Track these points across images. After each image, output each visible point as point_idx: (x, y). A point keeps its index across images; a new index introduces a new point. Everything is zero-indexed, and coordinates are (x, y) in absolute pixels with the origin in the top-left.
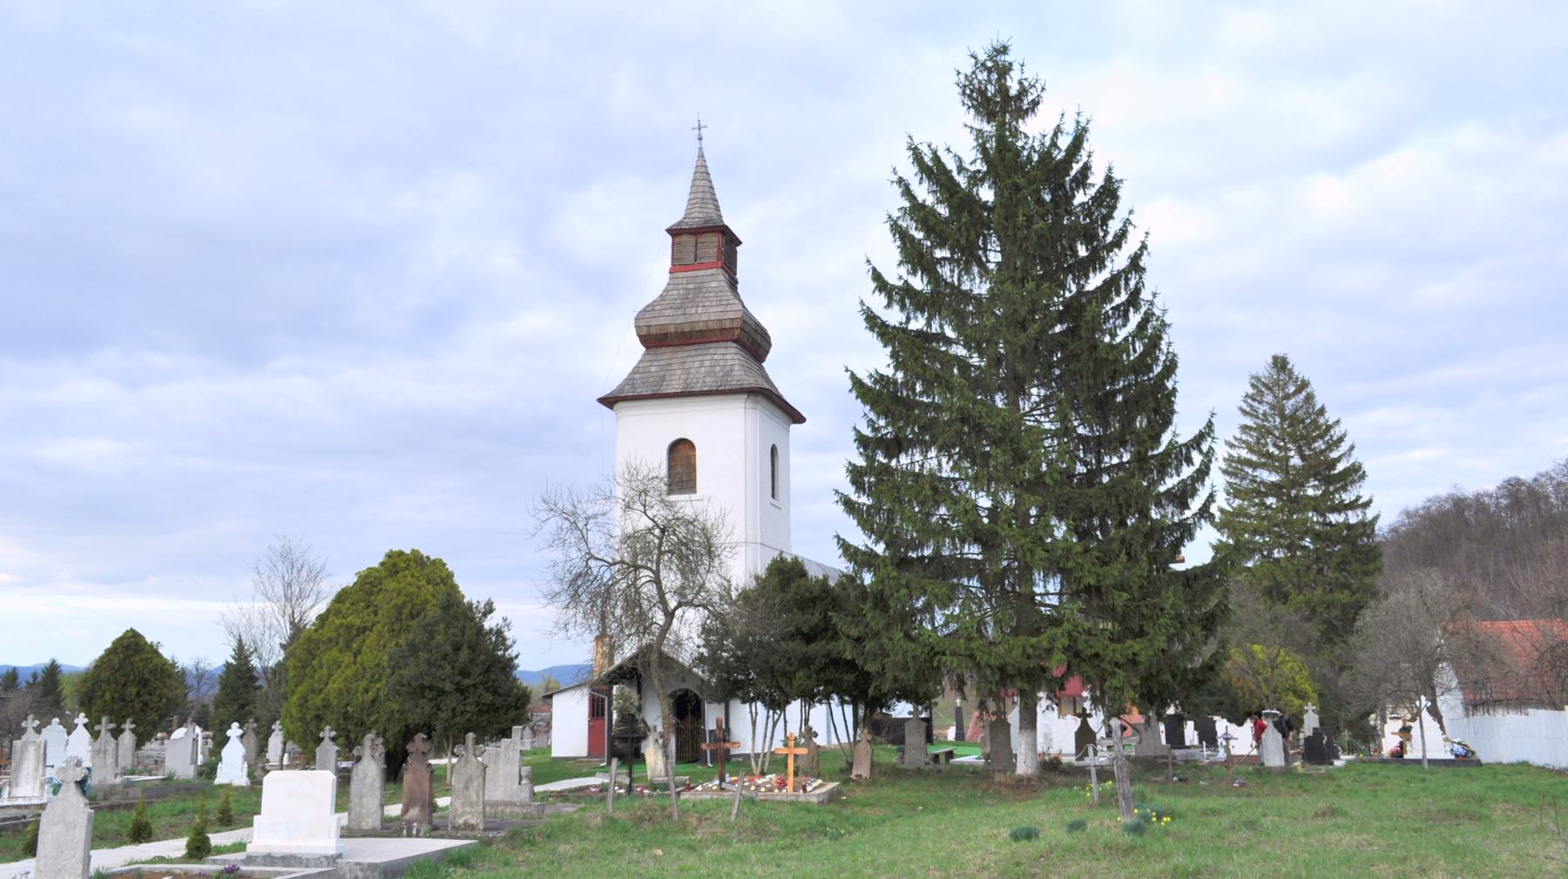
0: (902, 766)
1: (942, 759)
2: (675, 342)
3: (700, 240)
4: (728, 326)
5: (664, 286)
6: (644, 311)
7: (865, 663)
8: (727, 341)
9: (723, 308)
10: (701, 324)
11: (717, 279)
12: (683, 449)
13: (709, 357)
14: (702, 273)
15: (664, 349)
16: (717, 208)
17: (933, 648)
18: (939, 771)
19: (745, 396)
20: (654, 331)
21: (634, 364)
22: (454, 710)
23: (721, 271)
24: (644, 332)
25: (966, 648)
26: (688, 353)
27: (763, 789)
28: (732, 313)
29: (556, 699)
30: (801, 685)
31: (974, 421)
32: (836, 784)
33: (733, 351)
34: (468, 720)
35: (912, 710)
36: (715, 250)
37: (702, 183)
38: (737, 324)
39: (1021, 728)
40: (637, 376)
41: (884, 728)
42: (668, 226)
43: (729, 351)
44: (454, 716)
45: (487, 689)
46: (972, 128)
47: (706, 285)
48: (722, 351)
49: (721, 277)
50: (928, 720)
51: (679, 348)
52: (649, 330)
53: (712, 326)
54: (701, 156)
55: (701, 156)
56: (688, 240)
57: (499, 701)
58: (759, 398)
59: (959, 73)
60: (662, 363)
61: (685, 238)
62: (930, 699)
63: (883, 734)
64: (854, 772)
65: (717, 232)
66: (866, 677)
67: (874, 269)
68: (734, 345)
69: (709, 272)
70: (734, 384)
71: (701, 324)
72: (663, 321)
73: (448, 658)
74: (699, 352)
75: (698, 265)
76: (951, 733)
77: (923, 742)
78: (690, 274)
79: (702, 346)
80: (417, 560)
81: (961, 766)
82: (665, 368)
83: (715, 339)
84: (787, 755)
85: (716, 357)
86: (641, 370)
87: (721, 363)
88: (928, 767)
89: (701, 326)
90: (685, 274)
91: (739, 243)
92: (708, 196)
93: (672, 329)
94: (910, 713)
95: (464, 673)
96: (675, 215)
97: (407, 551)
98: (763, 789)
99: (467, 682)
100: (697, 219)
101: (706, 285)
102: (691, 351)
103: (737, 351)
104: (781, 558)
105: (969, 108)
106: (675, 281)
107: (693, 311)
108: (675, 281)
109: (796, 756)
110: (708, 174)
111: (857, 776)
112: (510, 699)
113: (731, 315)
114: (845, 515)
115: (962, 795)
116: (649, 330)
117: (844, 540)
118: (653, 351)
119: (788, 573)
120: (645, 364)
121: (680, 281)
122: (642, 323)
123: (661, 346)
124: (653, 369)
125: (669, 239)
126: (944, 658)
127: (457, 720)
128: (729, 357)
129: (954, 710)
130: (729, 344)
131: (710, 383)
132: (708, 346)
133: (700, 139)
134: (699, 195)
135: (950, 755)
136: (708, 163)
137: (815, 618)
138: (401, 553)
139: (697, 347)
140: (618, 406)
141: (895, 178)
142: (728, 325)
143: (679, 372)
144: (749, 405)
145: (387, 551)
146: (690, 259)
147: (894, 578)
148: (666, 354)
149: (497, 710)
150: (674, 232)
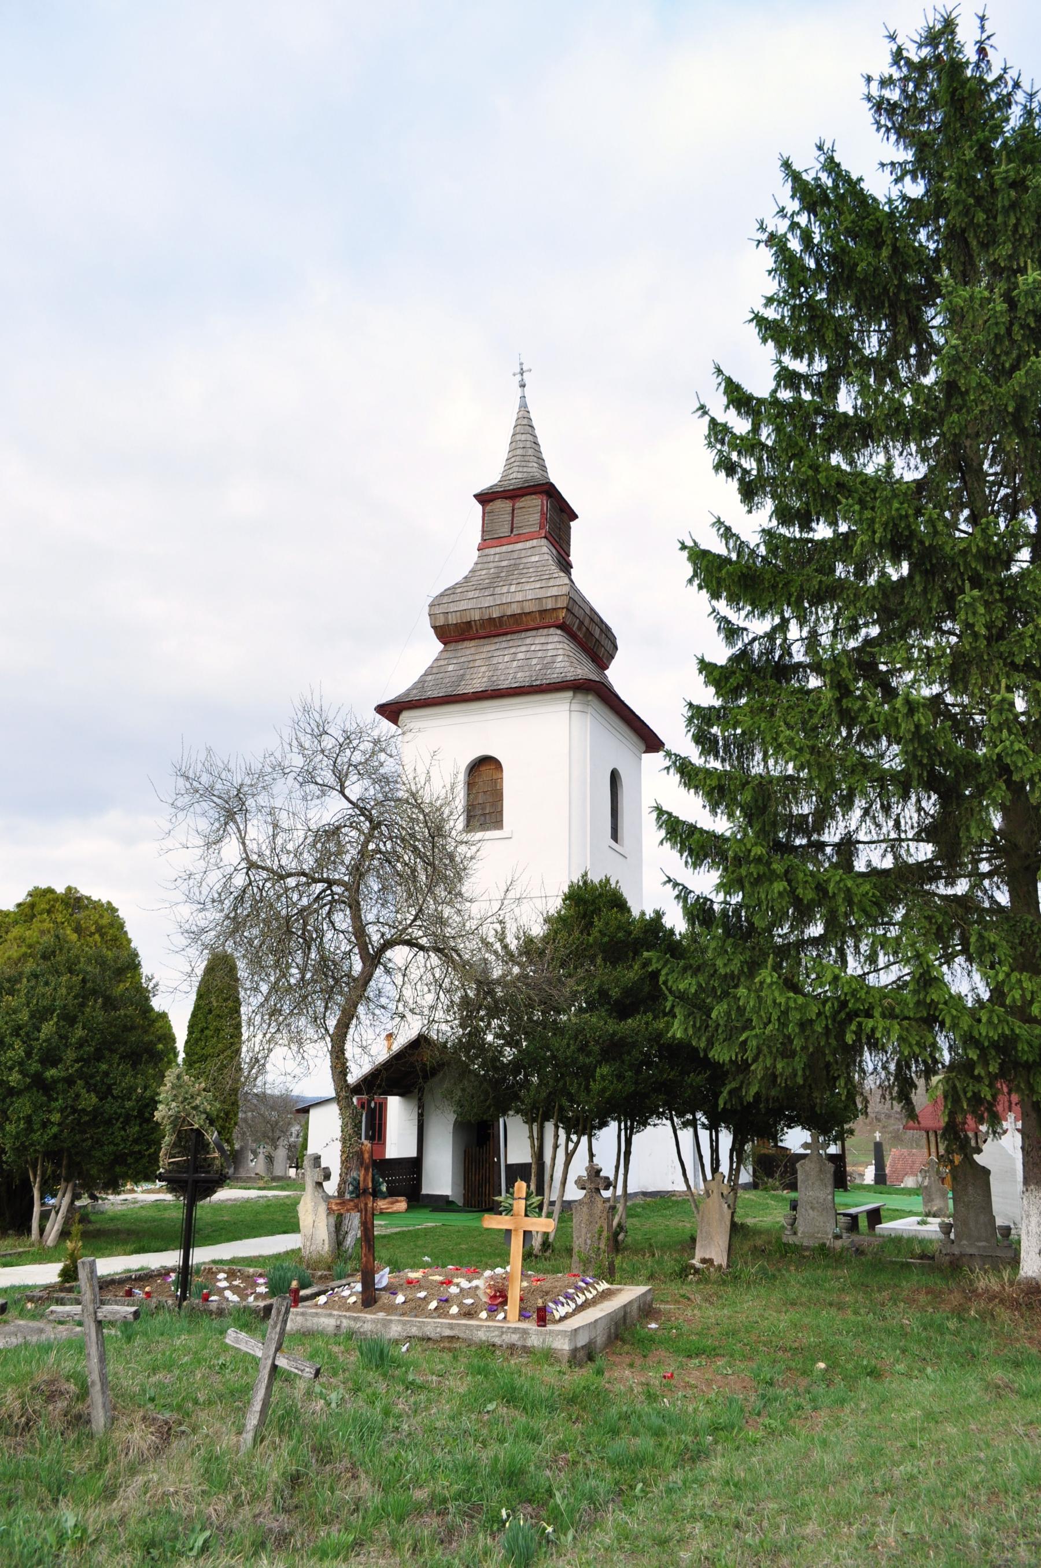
0: (792, 1240)
1: (863, 1223)
2: (482, 632)
3: (518, 505)
4: (549, 607)
5: (470, 566)
6: (442, 595)
7: (710, 1043)
8: (549, 627)
9: (543, 584)
10: (514, 606)
11: (541, 552)
12: (486, 770)
13: (524, 649)
14: (519, 546)
15: (467, 644)
16: (543, 468)
17: (844, 1004)
18: (859, 1252)
19: (569, 694)
20: (453, 620)
21: (429, 663)
22: (28, 1120)
23: (544, 542)
24: (441, 622)
25: (918, 1003)
26: (497, 646)
27: (454, 1310)
28: (556, 587)
29: (313, 1113)
30: (604, 1090)
31: (922, 543)
32: (642, 1289)
33: (556, 639)
34: (55, 1137)
35: (809, 1140)
36: (537, 516)
37: (523, 437)
38: (562, 603)
39: (1026, 1181)
40: (430, 678)
41: (778, 1166)
42: (477, 491)
43: (551, 639)
44: (30, 1129)
45: (90, 1088)
46: (893, 164)
47: (524, 560)
48: (543, 640)
49: (545, 549)
50: (839, 1160)
51: (486, 641)
52: (447, 619)
53: (529, 607)
54: (524, 406)
55: (524, 406)
56: (502, 506)
57: (110, 1107)
58: (590, 698)
59: (869, 79)
60: (463, 659)
61: (499, 505)
62: (841, 1123)
63: (777, 1176)
64: (699, 1254)
65: (540, 493)
66: (718, 1073)
67: (729, 381)
68: (559, 632)
69: (529, 544)
70: (554, 677)
71: (514, 606)
72: (463, 605)
73: (22, 1033)
74: (511, 644)
75: (514, 536)
76: (869, 1175)
77: (830, 1189)
78: (504, 549)
79: (514, 636)
80: (73, 901)
81: (897, 1241)
82: (466, 665)
83: (532, 625)
84: (508, 1232)
85: (533, 648)
86: (435, 671)
87: (540, 654)
88: (839, 1243)
89: (515, 609)
90: (498, 550)
91: (574, 516)
92: (530, 452)
93: (476, 616)
94: (806, 1146)
95: (50, 1058)
96: (490, 477)
97: (60, 889)
98: (454, 1310)
99: (52, 1072)
100: (517, 477)
101: (524, 560)
102: (502, 642)
103: (561, 639)
104: (585, 883)
105: (888, 130)
106: (485, 559)
107: (505, 589)
108: (485, 559)
109: (527, 1234)
110: (532, 427)
111: (704, 1261)
112: (128, 1104)
113: (554, 591)
114: (683, 790)
115: (910, 1320)
116: (447, 619)
117: (670, 814)
118: (452, 646)
119: (594, 901)
120: (442, 663)
121: (491, 558)
122: (437, 610)
123: (464, 640)
124: (451, 668)
125: (479, 507)
126: (870, 1023)
127: (35, 1137)
128: (550, 647)
129: (872, 1147)
130: (552, 630)
131: (522, 678)
132: (523, 635)
133: (523, 386)
134: (519, 452)
135: (875, 1216)
136: (532, 416)
137: (631, 974)
138: (50, 891)
139: (509, 637)
140: (405, 716)
141: (764, 237)
142: (550, 605)
143: (483, 669)
144: (575, 706)
145: (31, 888)
146: (505, 530)
147: (759, 860)
148: (468, 650)
149: (109, 1123)
150: (484, 498)
